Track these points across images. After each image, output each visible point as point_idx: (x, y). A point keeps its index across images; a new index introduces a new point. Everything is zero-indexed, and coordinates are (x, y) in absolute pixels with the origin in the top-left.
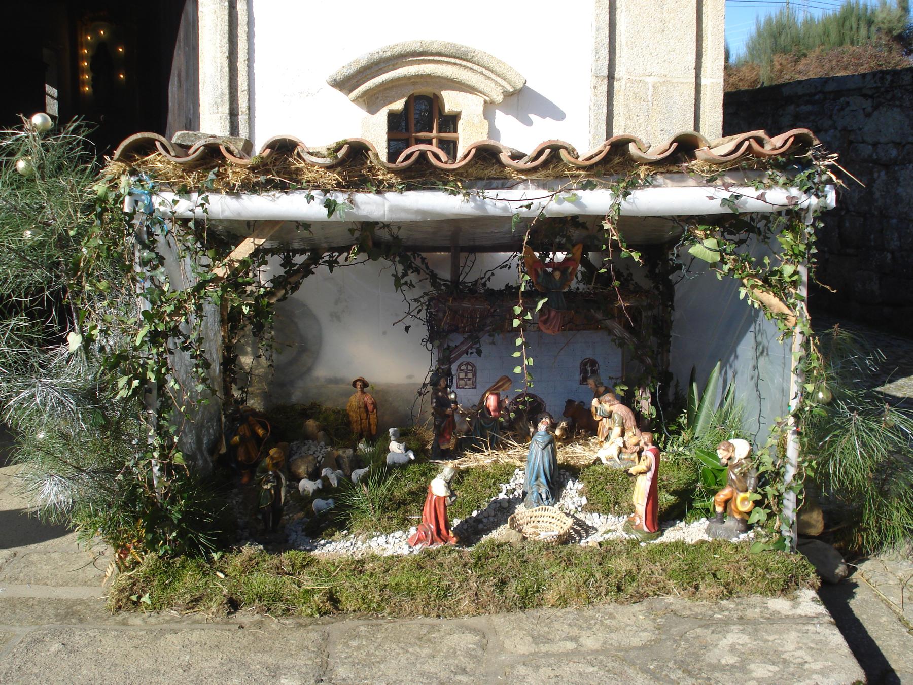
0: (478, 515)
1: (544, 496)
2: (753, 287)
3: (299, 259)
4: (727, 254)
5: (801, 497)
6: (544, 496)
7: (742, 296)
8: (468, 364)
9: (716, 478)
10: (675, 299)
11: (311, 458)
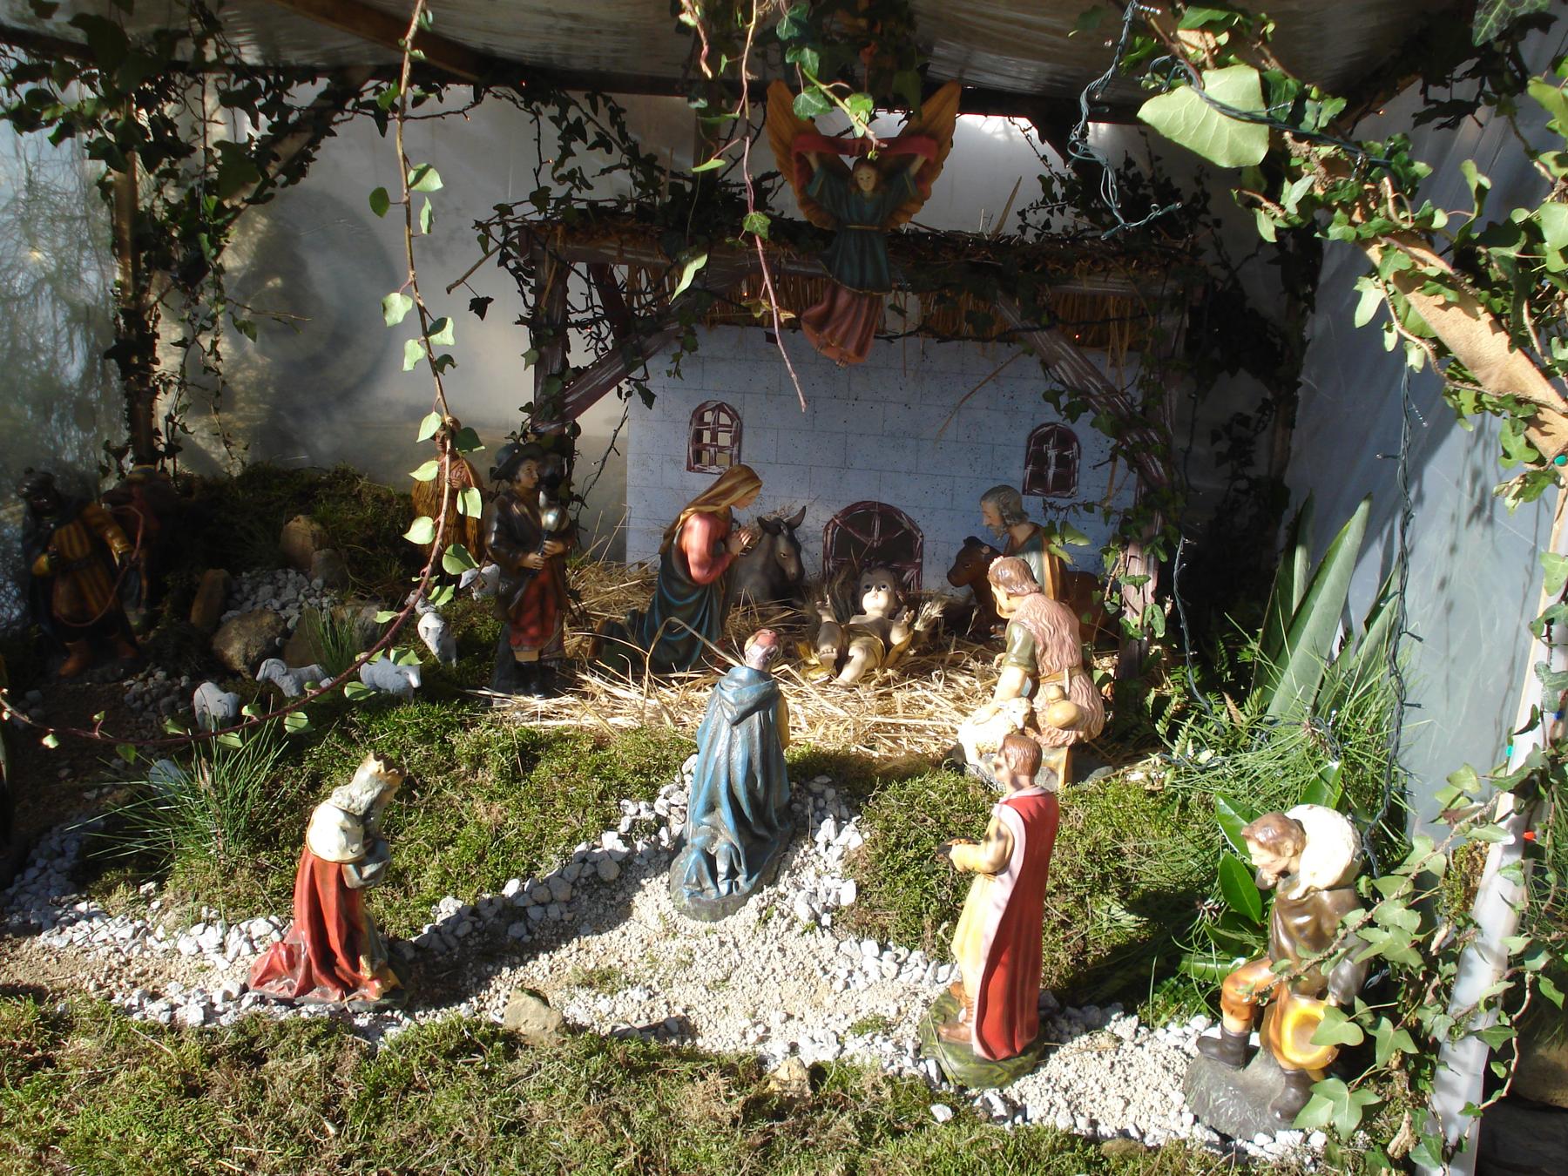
0: (519, 894)
1: (722, 867)
2: (1409, 280)
3: (304, 95)
4: (1299, 138)
5: (1500, 1071)
6: (722, 867)
7: (1364, 314)
8: (720, 408)
9: (1247, 919)
10: (1323, 278)
11: (268, 619)
